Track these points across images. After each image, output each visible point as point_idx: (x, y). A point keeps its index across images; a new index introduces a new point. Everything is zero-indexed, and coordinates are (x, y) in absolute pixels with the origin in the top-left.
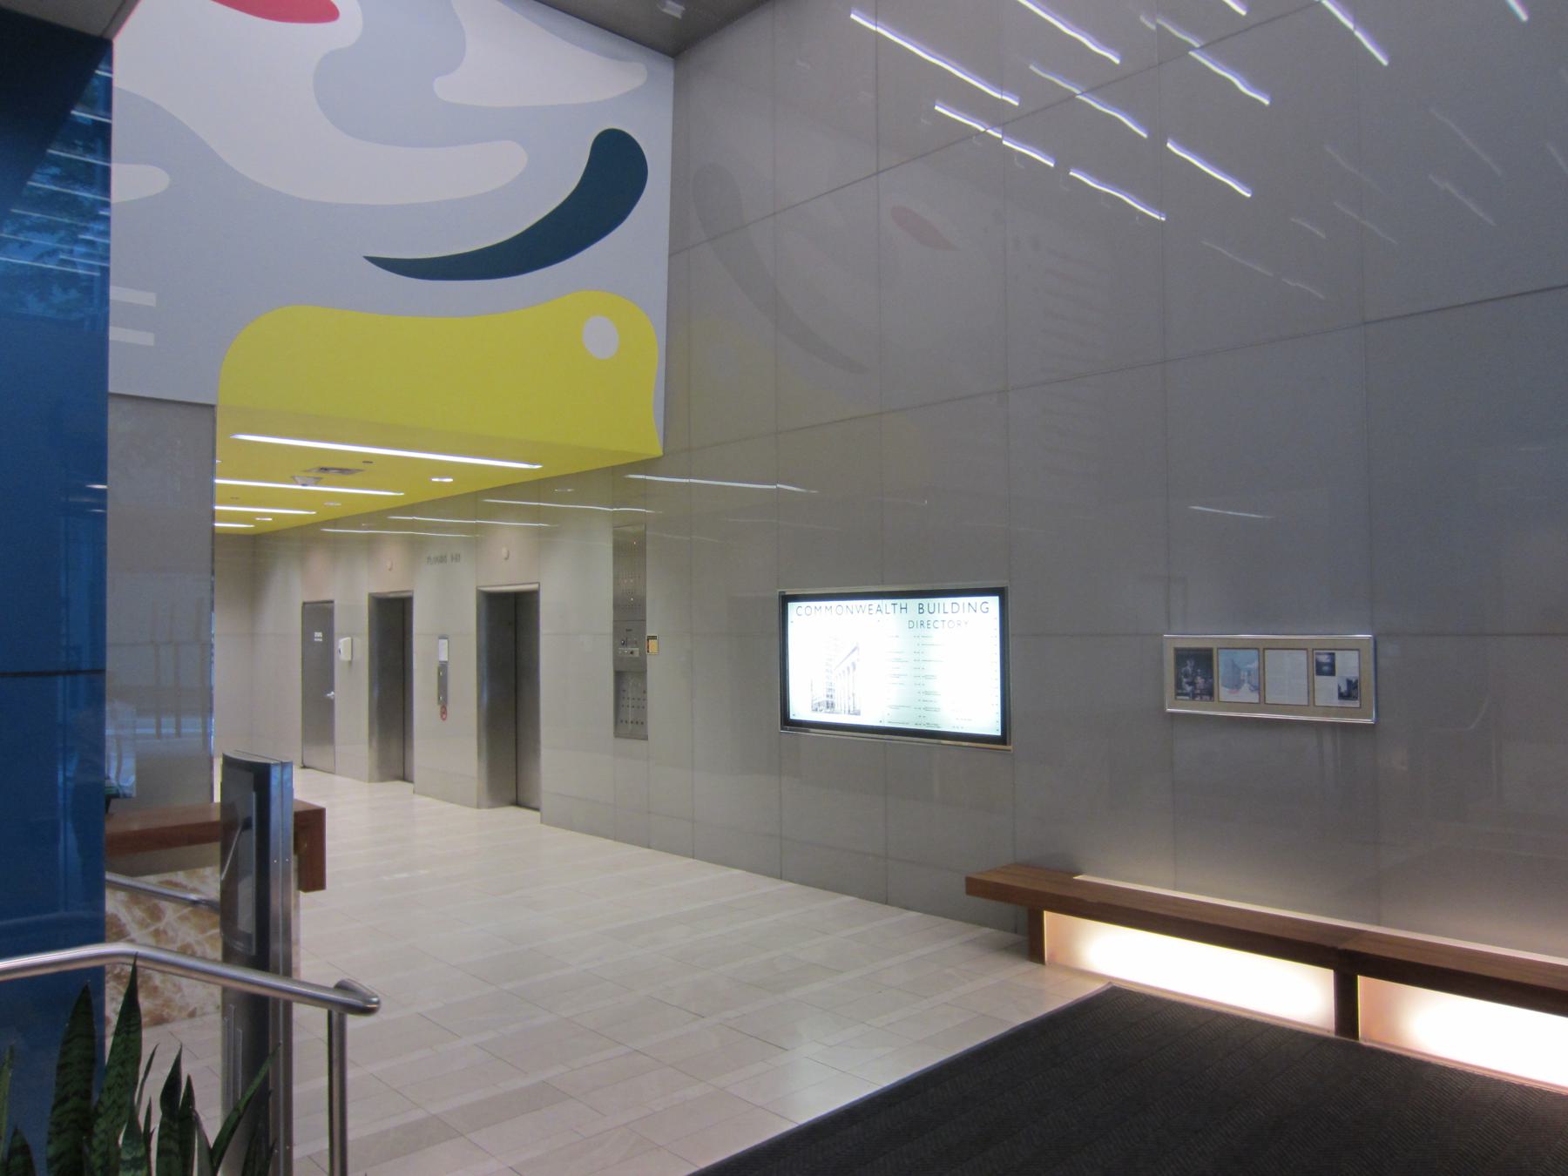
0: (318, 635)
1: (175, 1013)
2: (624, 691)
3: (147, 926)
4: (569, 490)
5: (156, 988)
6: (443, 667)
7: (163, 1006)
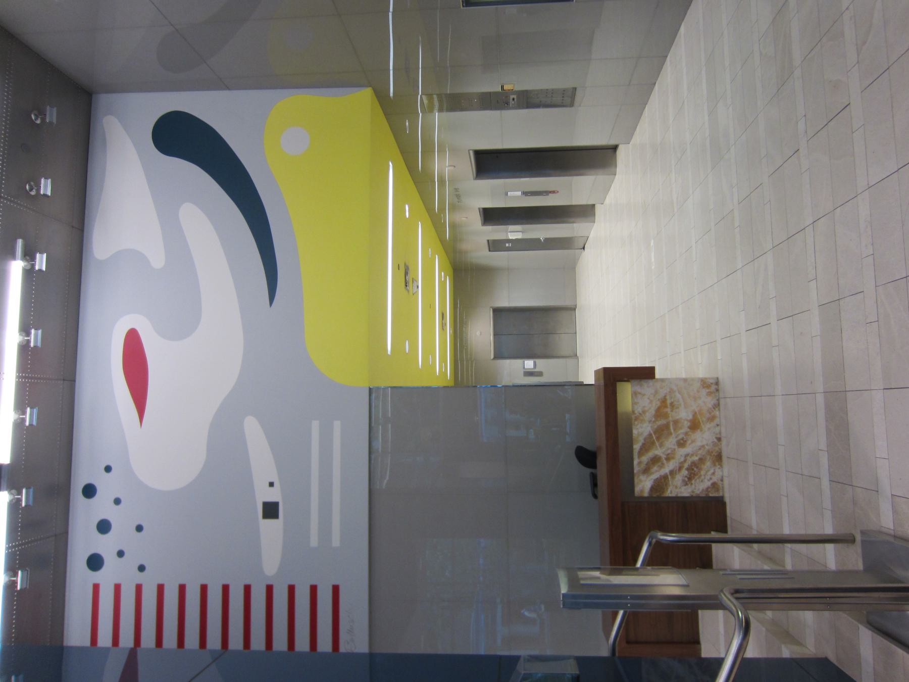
0: (507, 245)
1: (717, 449)
2: (541, 101)
3: (663, 464)
4: (407, 124)
5: (700, 459)
6: (525, 193)
7: (711, 455)
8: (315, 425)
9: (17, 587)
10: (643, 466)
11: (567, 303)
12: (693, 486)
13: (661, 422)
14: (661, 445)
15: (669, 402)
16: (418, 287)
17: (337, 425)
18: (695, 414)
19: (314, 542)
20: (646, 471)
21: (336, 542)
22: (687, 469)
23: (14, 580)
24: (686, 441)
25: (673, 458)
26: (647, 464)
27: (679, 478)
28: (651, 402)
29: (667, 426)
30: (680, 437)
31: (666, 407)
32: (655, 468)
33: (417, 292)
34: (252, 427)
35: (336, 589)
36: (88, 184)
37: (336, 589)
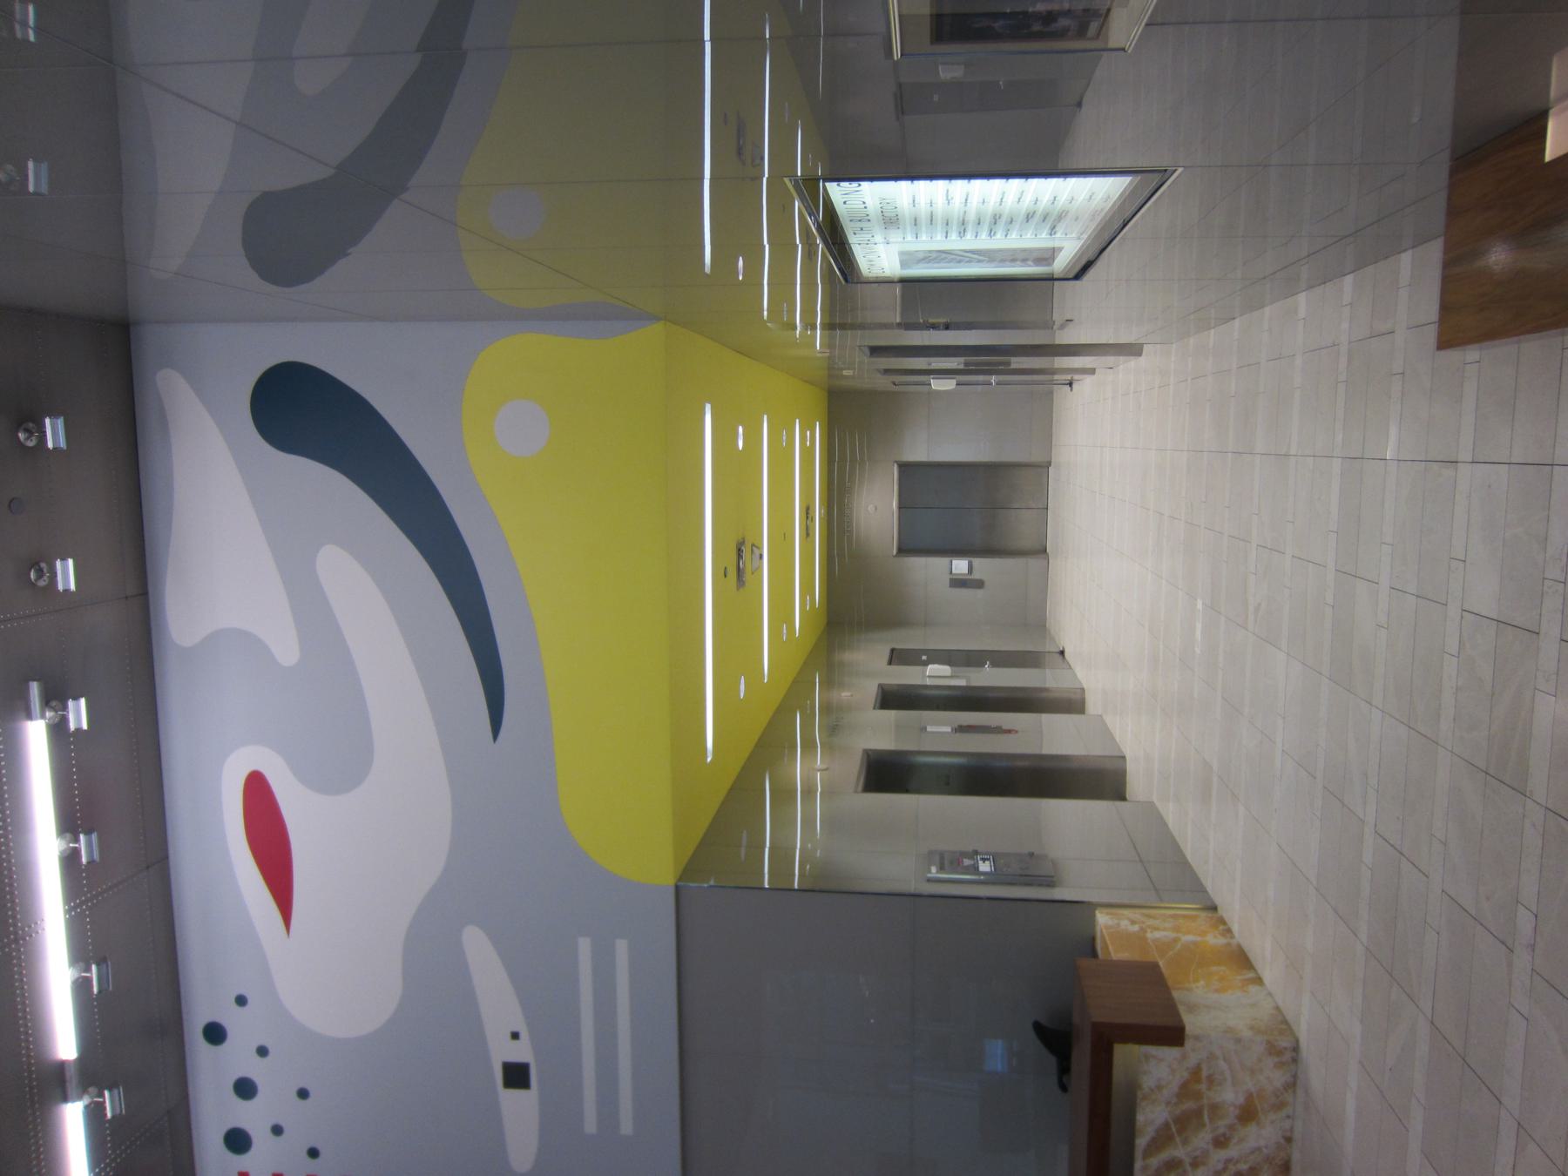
7: (1271, 1163)
8: (584, 946)
9: (106, 1115)
11: (1036, 457)
13: (1189, 1105)
14: (1185, 1142)
15: (1204, 1073)
16: (761, 557)
17: (622, 947)
18: (1249, 1097)
19: (590, 1126)
21: (627, 1127)
23: (76, 848)
25: (1204, 1164)
29: (1198, 1113)
30: (1221, 1130)
33: (760, 568)
34: (478, 948)
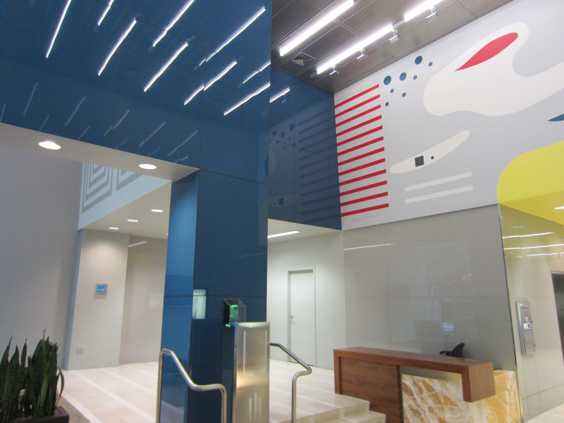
8: (469, 175)
10: (417, 382)
12: (408, 410)
13: (442, 400)
15: (454, 407)
17: (470, 188)
19: (407, 189)
20: (415, 384)
21: (408, 201)
22: (417, 410)
24: (432, 413)
26: (418, 384)
27: (412, 403)
28: (453, 395)
29: (440, 403)
31: (451, 405)
32: (417, 390)
34: (464, 135)
35: (386, 205)
36: (497, 9)
37: (386, 205)
